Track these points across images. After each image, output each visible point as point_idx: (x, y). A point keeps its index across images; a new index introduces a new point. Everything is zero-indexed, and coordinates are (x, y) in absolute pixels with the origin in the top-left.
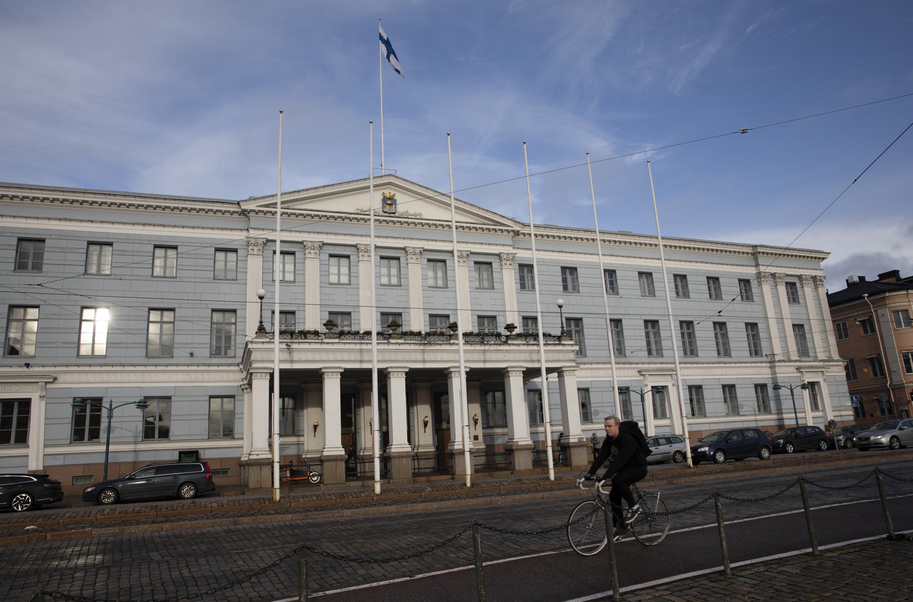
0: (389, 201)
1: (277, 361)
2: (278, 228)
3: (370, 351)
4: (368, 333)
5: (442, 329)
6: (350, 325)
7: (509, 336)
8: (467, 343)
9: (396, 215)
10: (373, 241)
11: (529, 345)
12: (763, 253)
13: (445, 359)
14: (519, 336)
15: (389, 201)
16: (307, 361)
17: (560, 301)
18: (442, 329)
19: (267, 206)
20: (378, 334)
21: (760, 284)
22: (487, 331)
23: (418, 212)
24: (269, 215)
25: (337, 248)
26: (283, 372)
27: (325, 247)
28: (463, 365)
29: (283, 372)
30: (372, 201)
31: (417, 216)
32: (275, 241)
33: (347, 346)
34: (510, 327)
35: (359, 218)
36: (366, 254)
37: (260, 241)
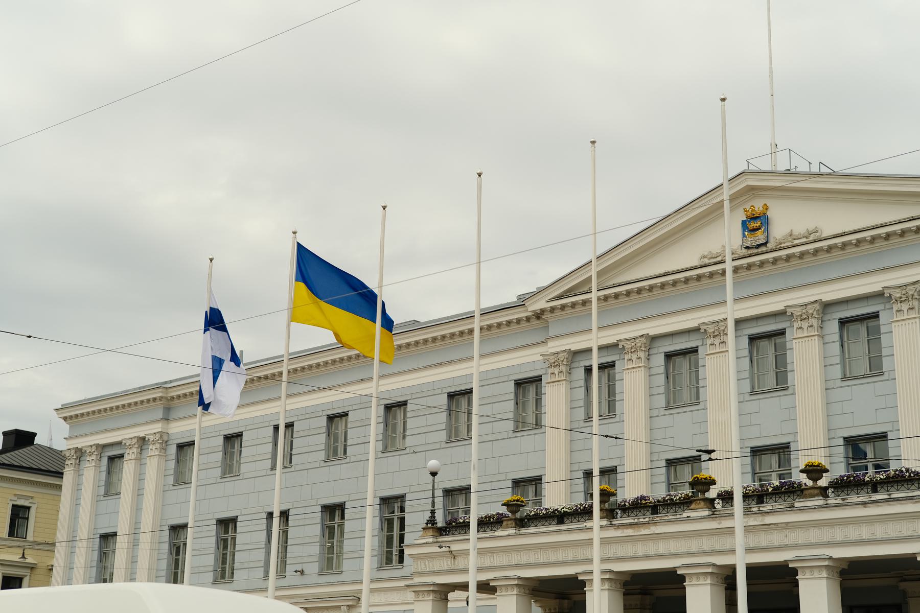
0: (756, 222)
1: (740, 551)
2: (594, 326)
3: (466, 553)
4: (727, 497)
5: (690, 489)
6: (538, 502)
7: (814, 485)
8: (747, 512)
9: (770, 246)
10: (732, 311)
11: (827, 506)
12: (179, 397)
13: (672, 551)
14: (841, 485)
15: (756, 222)
16: (646, 557)
17: (433, 464)
18: (690, 489)
19: (560, 297)
20: (746, 497)
21: (140, 460)
22: (777, 483)
23: (811, 227)
24: (579, 308)
25: (677, 340)
26: (753, 571)
27: (658, 343)
28: (596, 567)
29: (753, 571)
30: (726, 237)
31: (813, 236)
32: (590, 350)
33: (769, 519)
34: (814, 471)
35: (706, 276)
36: (717, 341)
37: (562, 356)
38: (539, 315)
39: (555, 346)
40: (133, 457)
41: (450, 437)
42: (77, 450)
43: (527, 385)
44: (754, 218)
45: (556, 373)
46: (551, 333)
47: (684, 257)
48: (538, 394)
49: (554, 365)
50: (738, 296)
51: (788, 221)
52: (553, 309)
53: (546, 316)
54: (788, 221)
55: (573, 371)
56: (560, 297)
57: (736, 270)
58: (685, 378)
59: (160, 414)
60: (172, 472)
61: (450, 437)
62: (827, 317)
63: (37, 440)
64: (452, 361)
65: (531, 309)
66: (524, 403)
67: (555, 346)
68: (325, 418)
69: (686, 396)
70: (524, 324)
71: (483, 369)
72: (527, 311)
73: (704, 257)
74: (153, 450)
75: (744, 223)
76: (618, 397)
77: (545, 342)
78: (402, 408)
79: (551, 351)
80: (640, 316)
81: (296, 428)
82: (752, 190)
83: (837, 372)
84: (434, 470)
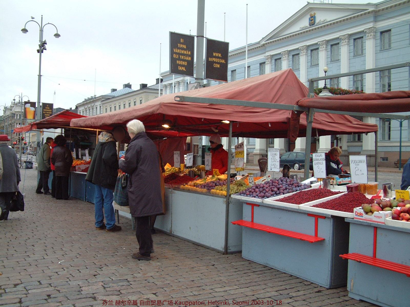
19: (268, 40)
30: (305, 23)
38: (264, 45)
39: (268, 54)
40: (182, 85)
41: (381, 49)
42: (178, 82)
43: (262, 64)
44: (312, 17)
45: (322, 47)
46: (267, 50)
47: (296, 28)
48: (390, 36)
49: (267, 59)
50: (249, 56)
51: (320, 18)
52: (266, 44)
53: (265, 45)
54: (320, 18)
55: (289, 56)
56: (268, 40)
57: (249, 50)
58: (387, 41)
59: (372, 19)
60: (352, 51)
61: (381, 49)
62: (350, 38)
63: (148, 86)
64: (341, 30)
65: (261, 44)
66: (357, 46)
67: (268, 54)
68: (259, 64)
69: (387, 46)
70: (261, 48)
71: (248, 61)
72: (260, 44)
73: (300, 28)
74: (182, 85)
75: (309, 18)
76: (364, 48)
77: (265, 53)
78: (280, 60)
79: (267, 55)
80: (346, 28)
81: (251, 67)
82: (311, 9)
83: (329, 60)
84: (326, 71)
